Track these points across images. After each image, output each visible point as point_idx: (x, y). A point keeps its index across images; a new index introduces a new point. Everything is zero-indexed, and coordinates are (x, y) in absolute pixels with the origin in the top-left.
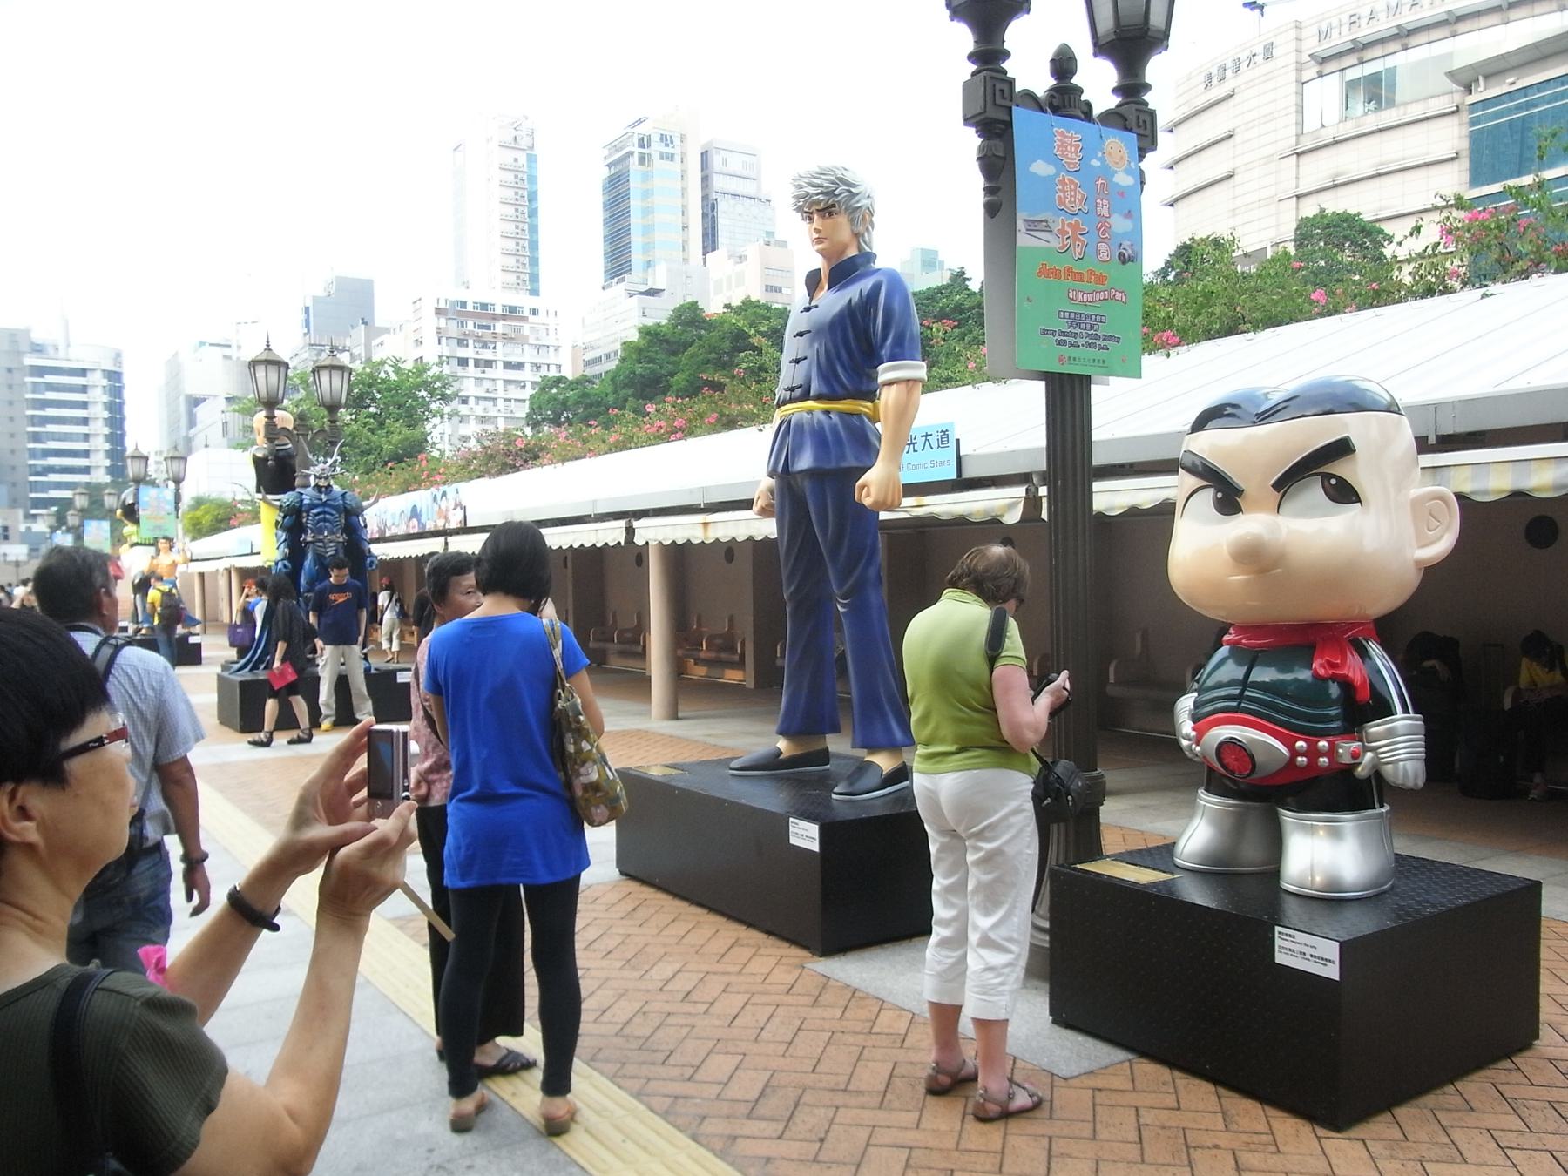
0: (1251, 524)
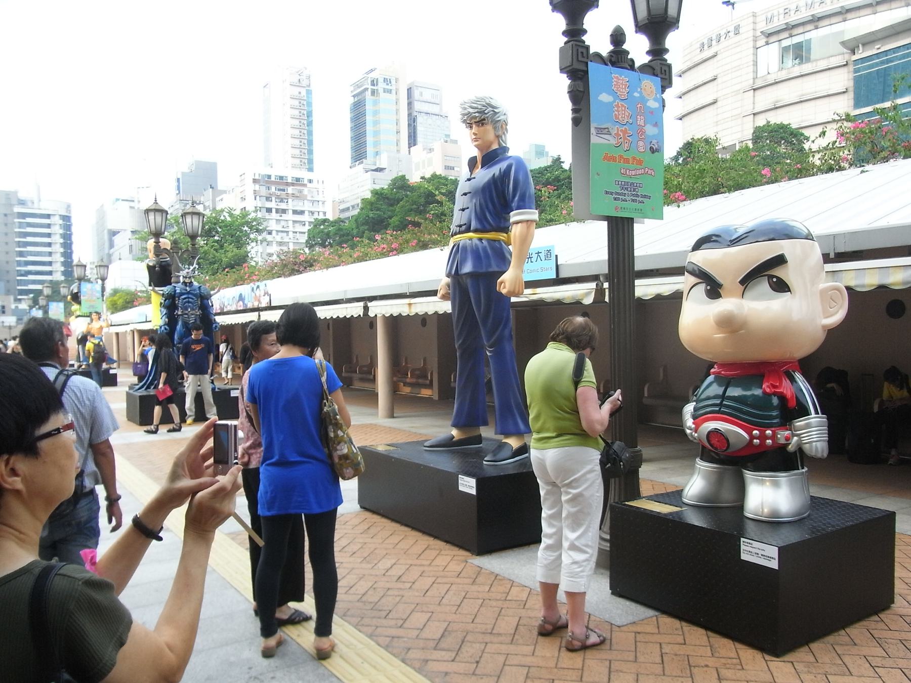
0: (727, 305)
